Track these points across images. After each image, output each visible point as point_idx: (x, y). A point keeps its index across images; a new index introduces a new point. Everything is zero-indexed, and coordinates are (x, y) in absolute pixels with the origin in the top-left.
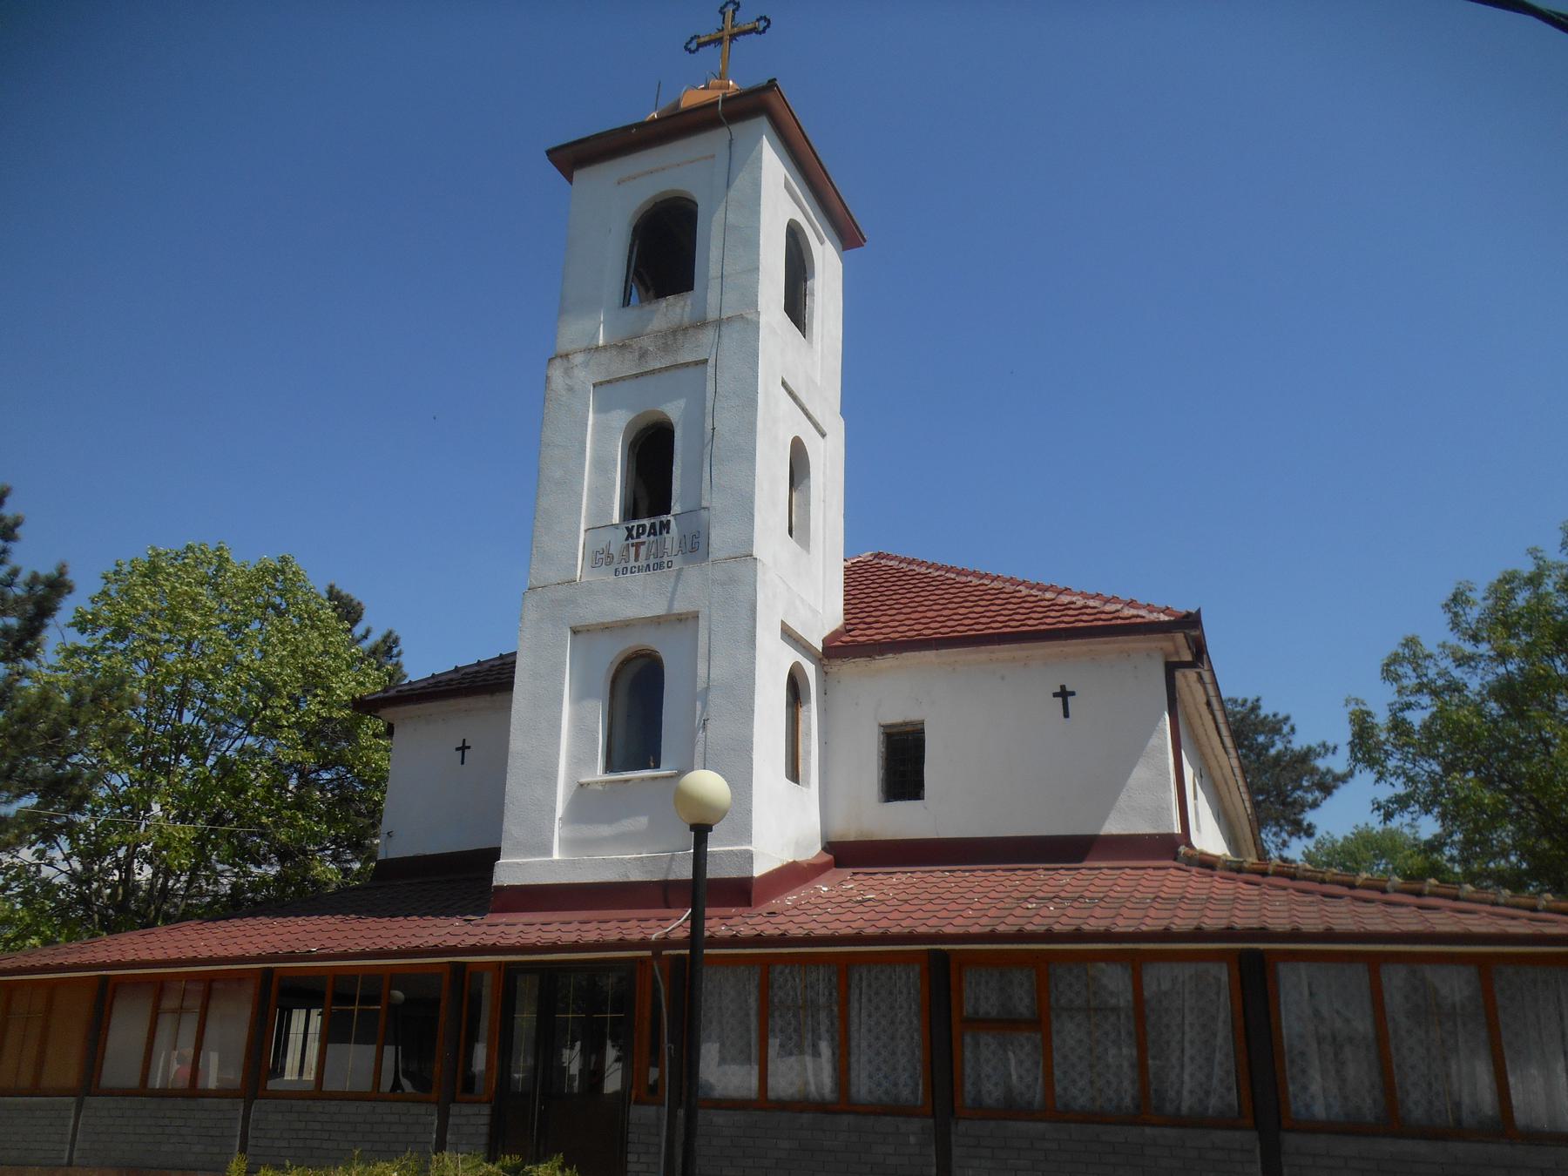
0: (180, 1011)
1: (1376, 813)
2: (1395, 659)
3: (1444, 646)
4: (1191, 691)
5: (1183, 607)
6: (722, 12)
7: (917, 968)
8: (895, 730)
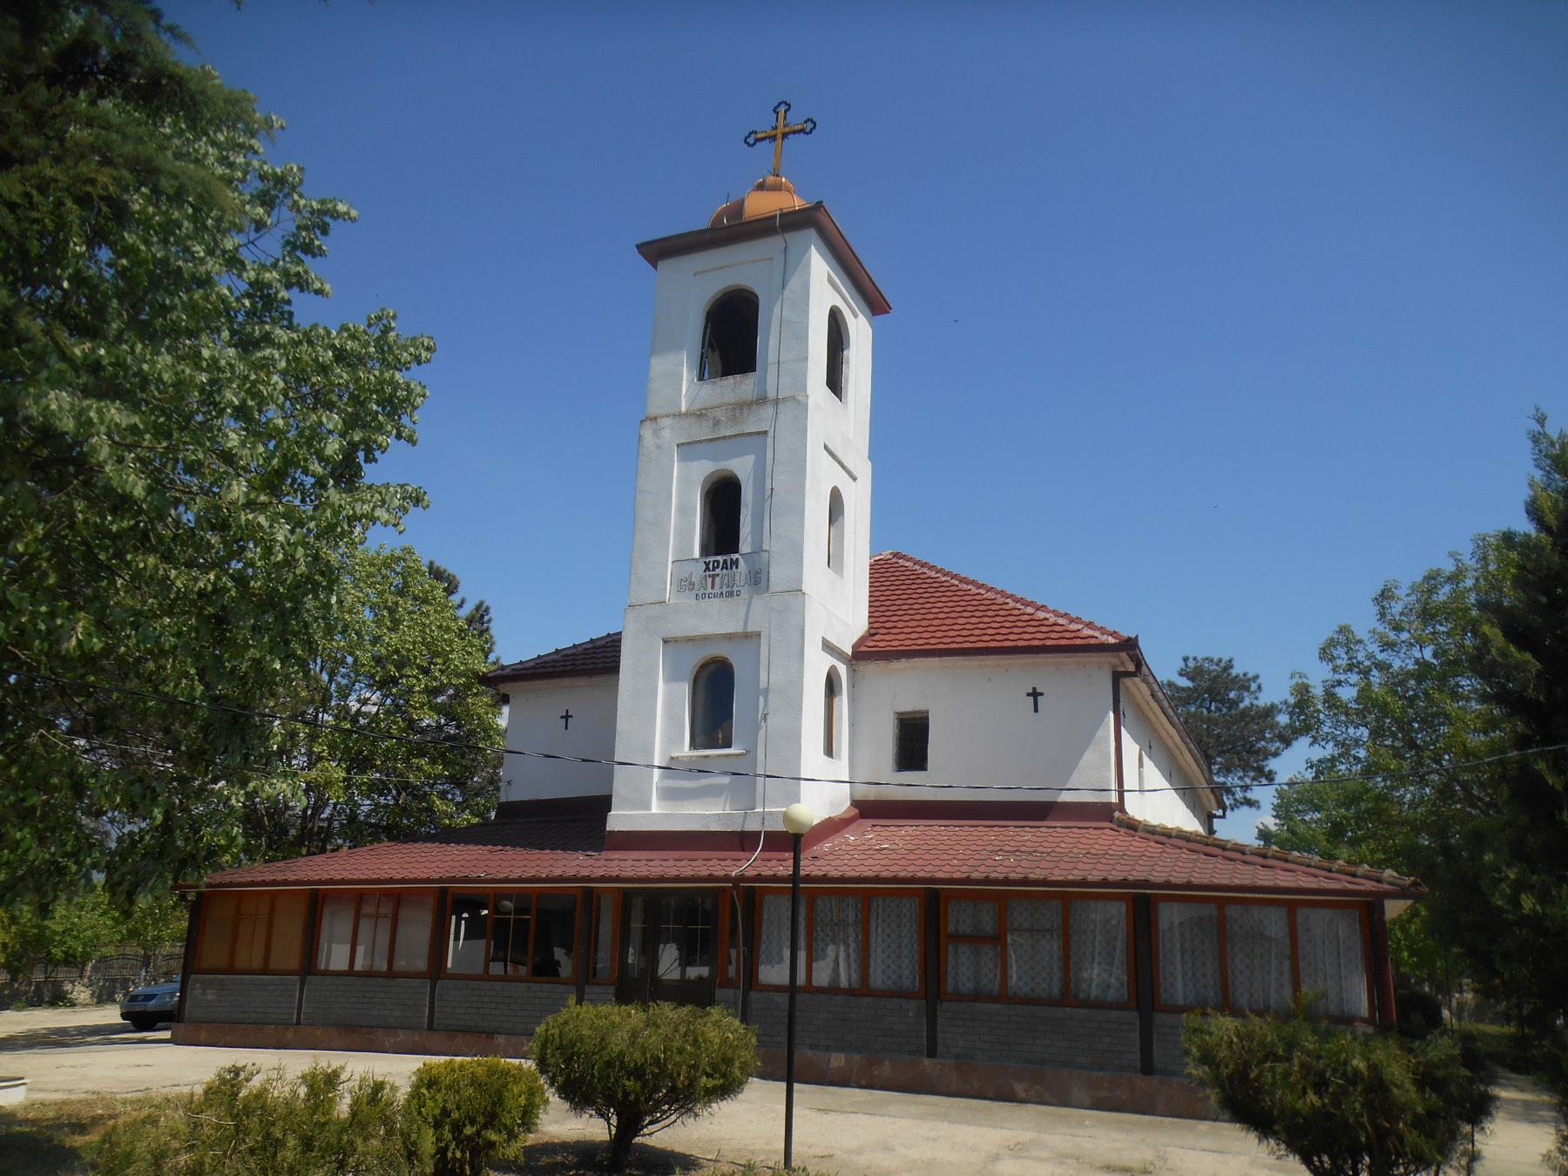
0: (377, 917)
1: (1309, 770)
2: (1332, 643)
3: (1374, 631)
4: (1138, 689)
5: (1126, 633)
6: (775, 111)
7: (917, 900)
8: (905, 717)
